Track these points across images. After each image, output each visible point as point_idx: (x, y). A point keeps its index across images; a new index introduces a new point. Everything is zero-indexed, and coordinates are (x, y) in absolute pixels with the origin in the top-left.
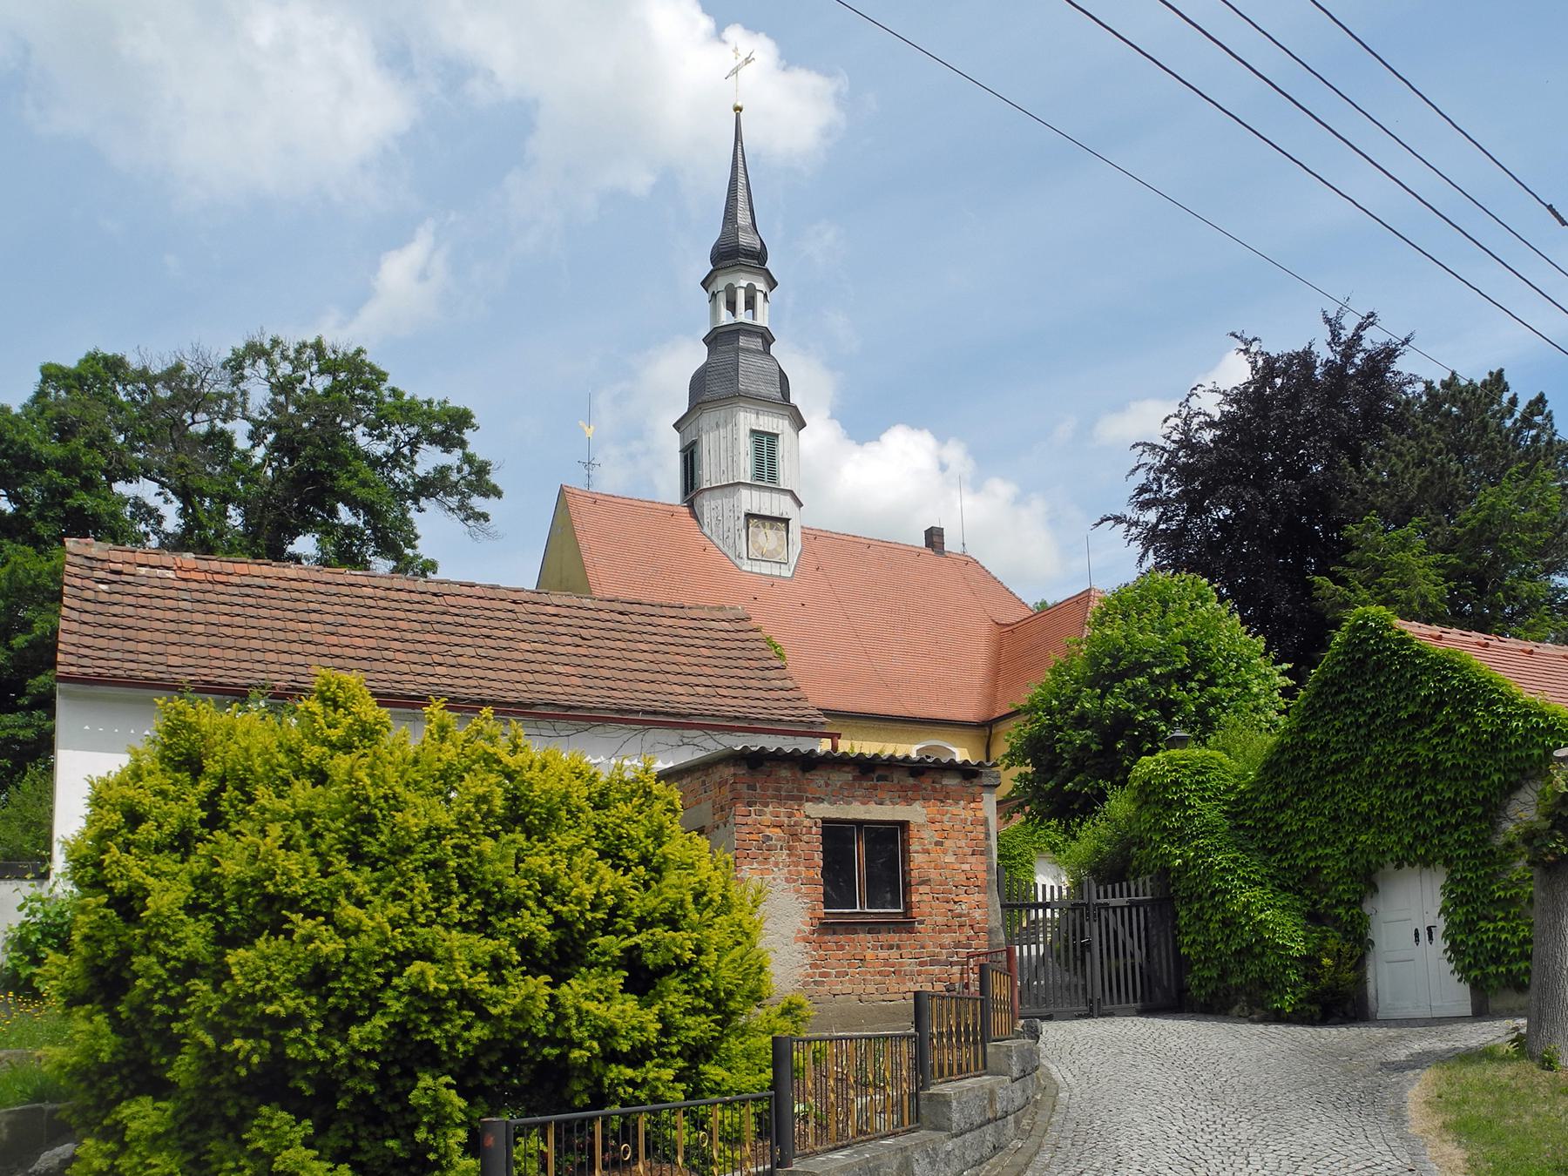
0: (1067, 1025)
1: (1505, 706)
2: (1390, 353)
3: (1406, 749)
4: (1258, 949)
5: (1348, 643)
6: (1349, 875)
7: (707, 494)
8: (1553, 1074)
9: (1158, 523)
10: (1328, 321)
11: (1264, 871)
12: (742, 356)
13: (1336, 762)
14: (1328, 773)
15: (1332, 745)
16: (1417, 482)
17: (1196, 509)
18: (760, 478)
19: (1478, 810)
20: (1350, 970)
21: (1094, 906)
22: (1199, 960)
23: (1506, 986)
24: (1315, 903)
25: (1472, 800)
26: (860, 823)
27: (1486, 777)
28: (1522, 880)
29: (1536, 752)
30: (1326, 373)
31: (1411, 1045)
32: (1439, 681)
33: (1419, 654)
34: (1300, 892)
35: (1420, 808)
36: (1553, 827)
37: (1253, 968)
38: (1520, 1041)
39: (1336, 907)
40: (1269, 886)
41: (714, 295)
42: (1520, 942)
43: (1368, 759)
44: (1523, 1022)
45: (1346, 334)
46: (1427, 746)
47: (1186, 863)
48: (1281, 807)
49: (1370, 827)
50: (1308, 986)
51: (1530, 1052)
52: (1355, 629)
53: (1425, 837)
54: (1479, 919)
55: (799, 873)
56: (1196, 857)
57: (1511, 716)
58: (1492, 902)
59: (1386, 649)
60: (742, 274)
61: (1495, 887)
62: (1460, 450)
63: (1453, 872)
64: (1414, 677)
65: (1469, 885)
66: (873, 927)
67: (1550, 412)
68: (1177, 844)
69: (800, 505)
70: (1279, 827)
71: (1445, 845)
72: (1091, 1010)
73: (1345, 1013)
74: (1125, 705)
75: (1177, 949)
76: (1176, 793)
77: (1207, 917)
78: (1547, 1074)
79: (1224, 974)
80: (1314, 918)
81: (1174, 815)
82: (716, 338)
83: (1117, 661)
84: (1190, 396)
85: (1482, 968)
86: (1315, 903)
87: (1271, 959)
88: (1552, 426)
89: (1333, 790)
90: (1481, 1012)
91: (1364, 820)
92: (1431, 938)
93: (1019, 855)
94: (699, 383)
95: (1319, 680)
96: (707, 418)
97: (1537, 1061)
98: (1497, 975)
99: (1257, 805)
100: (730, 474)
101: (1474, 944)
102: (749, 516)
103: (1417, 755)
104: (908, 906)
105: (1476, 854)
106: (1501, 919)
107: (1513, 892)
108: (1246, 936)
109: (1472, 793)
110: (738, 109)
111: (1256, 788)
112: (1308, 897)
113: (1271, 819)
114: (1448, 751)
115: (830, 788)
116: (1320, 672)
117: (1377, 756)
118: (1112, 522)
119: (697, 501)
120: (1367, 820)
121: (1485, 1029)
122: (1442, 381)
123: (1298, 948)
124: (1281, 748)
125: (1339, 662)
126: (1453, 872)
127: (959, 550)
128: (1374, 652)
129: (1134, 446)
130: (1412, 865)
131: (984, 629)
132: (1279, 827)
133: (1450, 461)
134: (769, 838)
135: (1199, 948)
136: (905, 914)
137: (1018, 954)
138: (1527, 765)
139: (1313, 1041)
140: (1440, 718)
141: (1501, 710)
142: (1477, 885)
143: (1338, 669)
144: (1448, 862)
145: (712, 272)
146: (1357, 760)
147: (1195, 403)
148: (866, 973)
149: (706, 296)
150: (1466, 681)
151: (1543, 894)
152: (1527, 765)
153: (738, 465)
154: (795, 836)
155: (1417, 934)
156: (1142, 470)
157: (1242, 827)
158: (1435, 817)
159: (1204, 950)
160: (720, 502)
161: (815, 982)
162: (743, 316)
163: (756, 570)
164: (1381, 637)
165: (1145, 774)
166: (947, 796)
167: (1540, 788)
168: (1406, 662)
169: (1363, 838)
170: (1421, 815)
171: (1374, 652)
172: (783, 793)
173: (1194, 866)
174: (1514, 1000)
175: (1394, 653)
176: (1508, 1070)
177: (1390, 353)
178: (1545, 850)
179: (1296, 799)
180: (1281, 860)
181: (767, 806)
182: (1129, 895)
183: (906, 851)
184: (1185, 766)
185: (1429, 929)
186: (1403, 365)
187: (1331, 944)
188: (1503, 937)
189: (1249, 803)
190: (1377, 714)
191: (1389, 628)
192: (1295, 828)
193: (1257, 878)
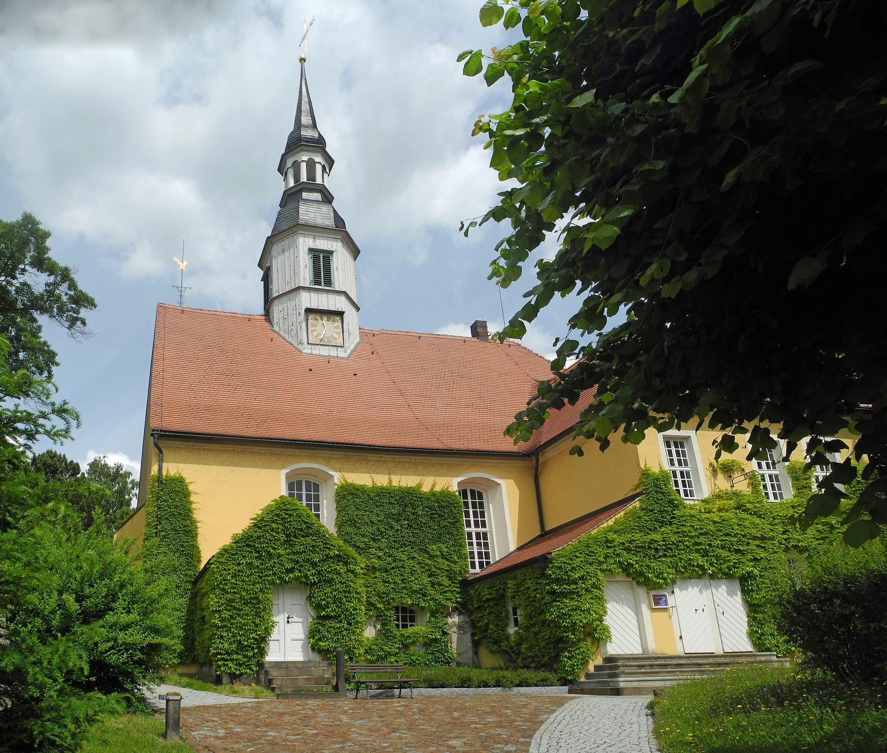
18: (318, 283)
60: (303, 153)
93: (582, 578)
102: (309, 311)
110: (303, 60)
153: (299, 276)
160: (285, 305)
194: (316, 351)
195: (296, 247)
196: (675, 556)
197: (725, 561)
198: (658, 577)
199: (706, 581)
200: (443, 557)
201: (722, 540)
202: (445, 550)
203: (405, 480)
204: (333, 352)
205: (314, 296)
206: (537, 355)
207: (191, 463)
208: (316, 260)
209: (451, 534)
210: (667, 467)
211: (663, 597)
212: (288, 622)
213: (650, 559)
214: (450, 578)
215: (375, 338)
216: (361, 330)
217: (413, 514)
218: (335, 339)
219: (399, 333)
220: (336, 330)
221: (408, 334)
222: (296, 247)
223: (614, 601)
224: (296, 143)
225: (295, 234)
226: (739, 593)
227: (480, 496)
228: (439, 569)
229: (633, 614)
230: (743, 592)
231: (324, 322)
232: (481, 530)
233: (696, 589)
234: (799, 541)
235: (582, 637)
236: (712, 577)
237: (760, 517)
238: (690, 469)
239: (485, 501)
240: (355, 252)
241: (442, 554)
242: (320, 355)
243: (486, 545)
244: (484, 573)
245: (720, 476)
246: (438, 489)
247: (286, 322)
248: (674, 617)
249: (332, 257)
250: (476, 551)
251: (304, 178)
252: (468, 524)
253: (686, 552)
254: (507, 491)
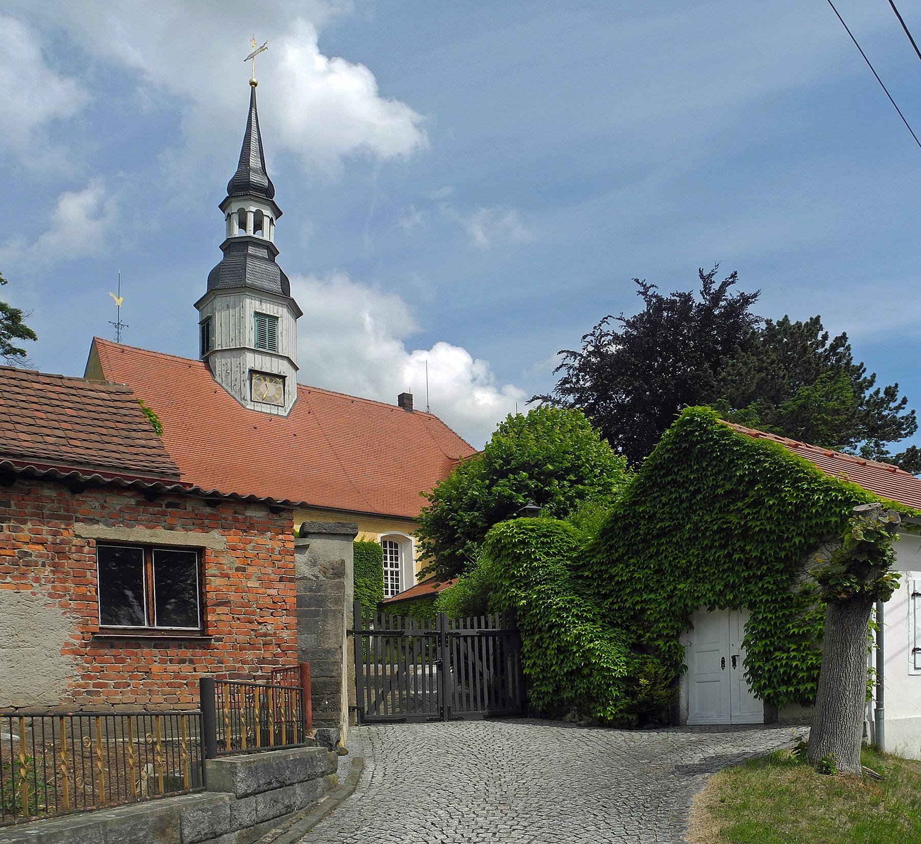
0: (416, 727)
1: (809, 484)
2: (746, 300)
3: (720, 519)
4: (586, 671)
5: (677, 435)
6: (668, 615)
7: (219, 355)
8: (829, 777)
9: (575, 404)
10: (702, 277)
11: (596, 610)
12: (249, 261)
13: (661, 528)
14: (654, 538)
15: (658, 515)
16: (755, 381)
17: (603, 395)
19: (781, 566)
20: (664, 687)
21: (446, 635)
22: (538, 679)
23: (794, 701)
24: (640, 636)
25: (776, 558)
26: (149, 547)
27: (788, 540)
28: (814, 620)
29: (833, 519)
30: (699, 311)
31: (707, 749)
32: (753, 464)
33: (737, 443)
34: (627, 628)
35: (731, 565)
36: (847, 572)
37: (582, 686)
38: (803, 749)
39: (656, 639)
40: (600, 622)
41: (229, 216)
42: (808, 668)
43: (688, 527)
44: (805, 730)
45: (715, 287)
46: (739, 516)
47: (529, 604)
48: (614, 563)
49: (688, 578)
50: (628, 700)
51: (810, 758)
52: (684, 423)
53: (734, 586)
54: (775, 650)
55: (66, 590)
56: (537, 600)
57: (813, 491)
58: (787, 637)
59: (709, 440)
61: (790, 625)
62: (786, 361)
63: (755, 613)
64: (732, 461)
65: (769, 623)
66: (160, 643)
67: (849, 345)
68: (523, 589)
69: (297, 369)
70: (612, 577)
71: (750, 592)
72: (442, 715)
73: (660, 720)
74: (508, 492)
75: (521, 669)
76: (523, 549)
77: (545, 645)
78: (825, 777)
79: (558, 690)
80: (638, 647)
81: (522, 566)
82: (229, 246)
83: (507, 462)
84: (603, 322)
85: (775, 688)
86: (640, 636)
87: (597, 679)
88: (850, 354)
89: (658, 550)
90: (771, 721)
91: (683, 573)
92: (734, 664)
94: (214, 278)
95: (651, 465)
96: (219, 302)
97: (816, 766)
98: (787, 693)
99: (595, 560)
100: (238, 341)
101: (769, 670)
102: (252, 372)
103: (730, 522)
104: (205, 624)
105: (776, 599)
106: (793, 650)
107: (805, 629)
108: (577, 661)
109: (775, 552)
110: (254, 85)
111: (594, 549)
112: (634, 632)
113: (606, 571)
114: (757, 519)
115: (106, 511)
116: (652, 459)
117: (696, 524)
119: (211, 359)
120: (686, 573)
121: (773, 736)
122: (778, 321)
123: (621, 670)
124: (615, 518)
125: (668, 451)
126: (755, 613)
127: (424, 410)
128: (698, 442)
129: (560, 353)
130: (722, 608)
131: (440, 461)
132: (612, 577)
133: (780, 368)
134: (27, 554)
135: (538, 670)
136: (202, 632)
137: (365, 673)
138: (825, 531)
139: (623, 744)
140: (751, 493)
141: (805, 486)
142: (775, 623)
143: (667, 456)
144: (752, 606)
145: (227, 198)
146: (679, 527)
147: (605, 328)
148: (152, 684)
149: (223, 216)
150: (777, 464)
151: (833, 628)
152: (825, 531)
154: (61, 554)
155: (723, 662)
156: (564, 368)
157: (581, 577)
158: (743, 571)
159: (542, 671)
160: (229, 360)
161: (89, 693)
162: (250, 232)
163: (258, 409)
164: (705, 429)
165: (498, 535)
166: (252, 527)
167: (834, 549)
168: (725, 449)
169: (681, 586)
170: (730, 569)
171: (698, 442)
172: (46, 512)
173: (536, 606)
174: (800, 712)
175: (716, 442)
176: (789, 774)
177: (746, 300)
178: (839, 588)
179: (626, 558)
180: (612, 603)
181: (25, 523)
182: (479, 627)
183: (202, 574)
184: (532, 530)
185: (734, 658)
186: (751, 309)
187: (649, 668)
188: (794, 664)
189: (588, 559)
190: (698, 491)
191: (713, 423)
192: (625, 578)
193: (589, 615)
195: (242, 307)
200: (367, 587)
202: (369, 582)
204: (274, 411)
214: (370, 601)
215: (311, 395)
218: (277, 399)
219: (334, 394)
222: (242, 307)
225: (241, 293)
227: (396, 547)
228: (363, 595)
232: (394, 569)
239: (399, 549)
241: (366, 585)
242: (261, 412)
243: (397, 579)
244: (395, 599)
246: (365, 541)
247: (230, 376)
250: (389, 583)
252: (386, 565)
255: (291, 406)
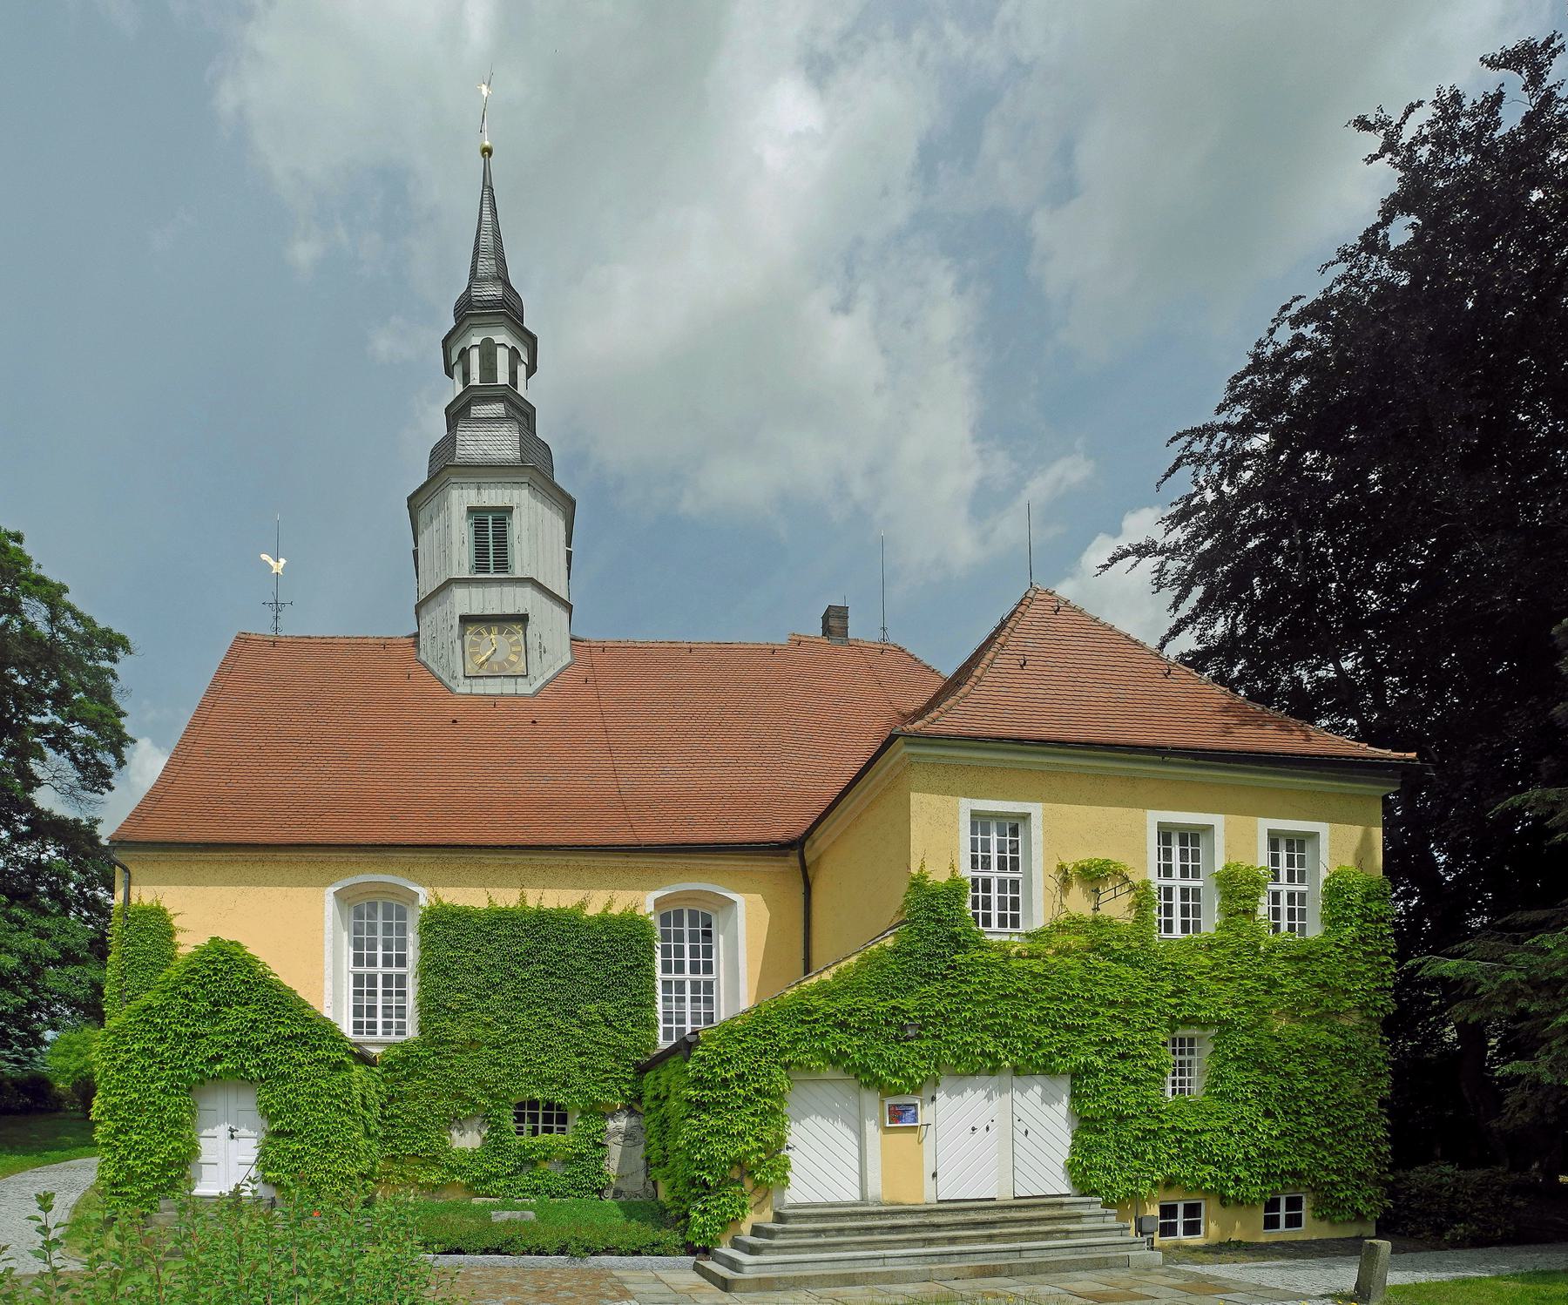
60: (474, 331)
102: (466, 620)
118: (1132, 559)
129: (1174, 439)
160: (433, 614)
194: (480, 687)
196: (939, 1037)
197: (1039, 1045)
198: (895, 1074)
199: (1006, 1079)
201: (1042, 1008)
203: (554, 898)
204: (508, 687)
205: (476, 592)
206: (928, 668)
207: (176, 884)
208: (480, 528)
209: (626, 985)
210: (966, 872)
211: (911, 1108)
212: (232, 1137)
213: (887, 1043)
216: (573, 642)
217: (558, 953)
218: (512, 664)
219: (657, 645)
220: (513, 649)
221: (673, 645)
223: (818, 1114)
224: (468, 312)
226: (1066, 1099)
229: (852, 1136)
230: (1074, 1096)
231: (492, 636)
233: (981, 1093)
234: (1199, 1007)
235: (737, 1177)
236: (1016, 1070)
237: (1135, 965)
238: (1021, 876)
239: (713, 929)
240: (567, 506)
245: (1076, 890)
246: (615, 911)
248: (928, 1142)
249: (511, 518)
251: (475, 380)
253: (963, 1030)
254: (748, 913)
255: (549, 675)
